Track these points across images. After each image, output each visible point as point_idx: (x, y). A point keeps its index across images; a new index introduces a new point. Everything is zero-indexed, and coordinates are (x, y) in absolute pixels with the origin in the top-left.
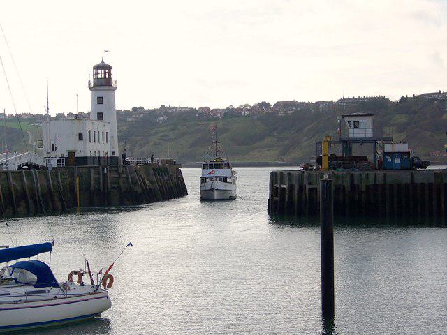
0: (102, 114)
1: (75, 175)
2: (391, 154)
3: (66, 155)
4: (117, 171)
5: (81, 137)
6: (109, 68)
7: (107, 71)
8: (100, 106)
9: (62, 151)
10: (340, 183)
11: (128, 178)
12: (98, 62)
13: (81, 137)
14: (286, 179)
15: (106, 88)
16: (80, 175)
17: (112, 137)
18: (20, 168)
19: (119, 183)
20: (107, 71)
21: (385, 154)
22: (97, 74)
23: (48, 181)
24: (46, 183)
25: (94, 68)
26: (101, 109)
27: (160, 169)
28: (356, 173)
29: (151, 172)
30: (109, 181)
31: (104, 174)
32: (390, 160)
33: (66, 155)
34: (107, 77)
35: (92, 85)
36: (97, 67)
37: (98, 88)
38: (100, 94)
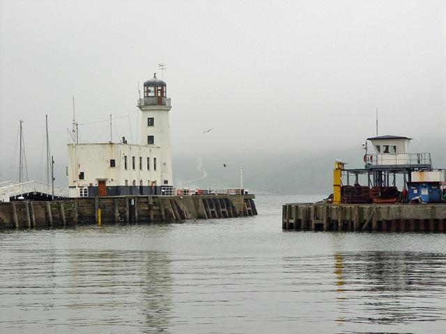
0: (153, 137)
1: (97, 207)
2: (418, 185)
3: (95, 184)
4: (147, 203)
5: (113, 163)
6: (163, 85)
7: (160, 88)
8: (151, 128)
9: (91, 180)
10: (348, 217)
11: (160, 211)
12: (150, 78)
13: (113, 163)
14: (294, 211)
15: (157, 107)
16: (103, 207)
17: (165, 164)
18: (12, 199)
19: (149, 216)
20: (160, 88)
21: (410, 184)
22: (149, 91)
23: (47, 213)
24: (44, 216)
25: (145, 86)
26: (151, 131)
27: (215, 200)
28: (366, 207)
29: (201, 203)
30: (137, 214)
31: (131, 207)
32: (416, 192)
33: (95, 184)
34: (159, 95)
35: (143, 104)
36: (147, 85)
37: (149, 108)
38: (151, 115)
